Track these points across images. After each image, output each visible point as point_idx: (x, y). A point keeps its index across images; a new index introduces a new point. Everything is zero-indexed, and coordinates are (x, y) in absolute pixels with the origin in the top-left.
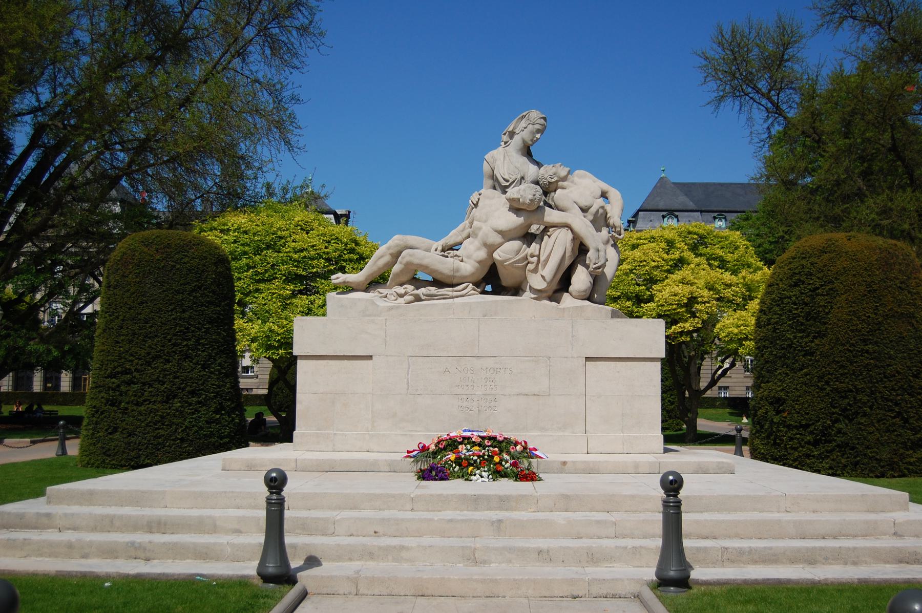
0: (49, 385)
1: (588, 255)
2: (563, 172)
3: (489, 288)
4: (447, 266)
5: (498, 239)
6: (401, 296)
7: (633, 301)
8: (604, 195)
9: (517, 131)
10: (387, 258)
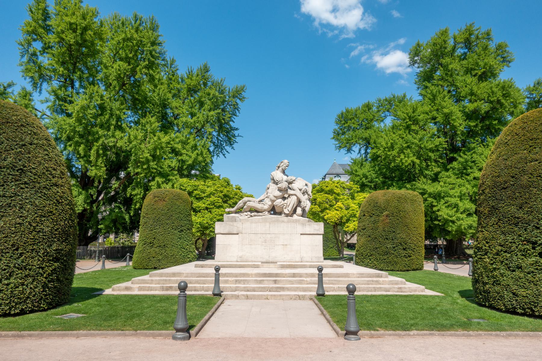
2: (294, 178)
3: (272, 212)
4: (259, 206)
6: (247, 215)
7: (315, 216)
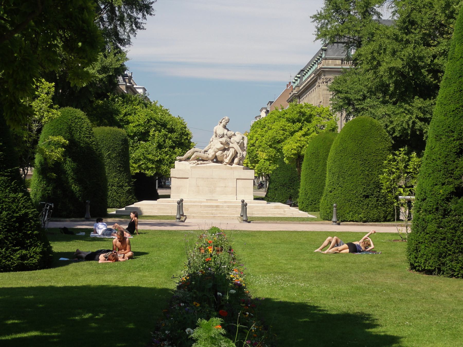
4: (205, 156)
5: (217, 150)
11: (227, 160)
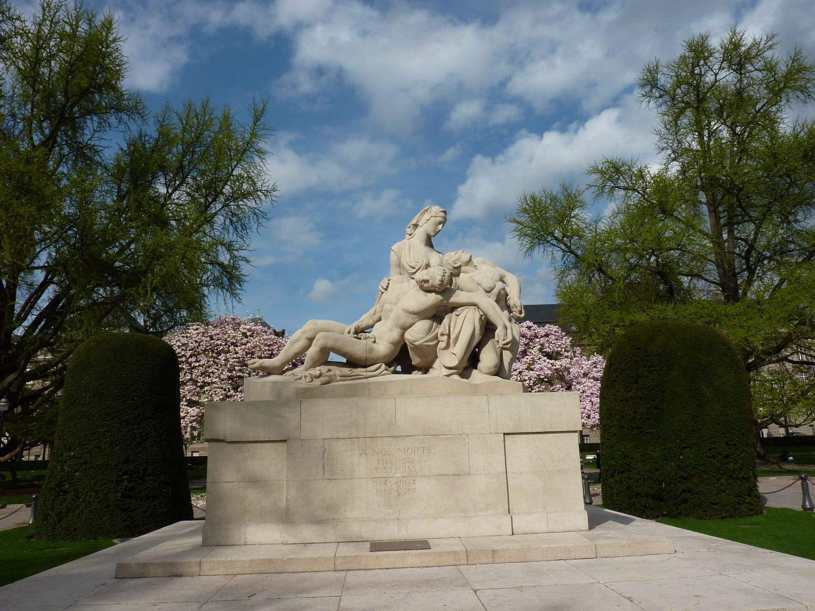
0: (590, 457)
1: (497, 332)
3: (399, 368)
4: (359, 348)
8: (502, 280)
9: (420, 224)
10: (302, 343)
11: (451, 356)
